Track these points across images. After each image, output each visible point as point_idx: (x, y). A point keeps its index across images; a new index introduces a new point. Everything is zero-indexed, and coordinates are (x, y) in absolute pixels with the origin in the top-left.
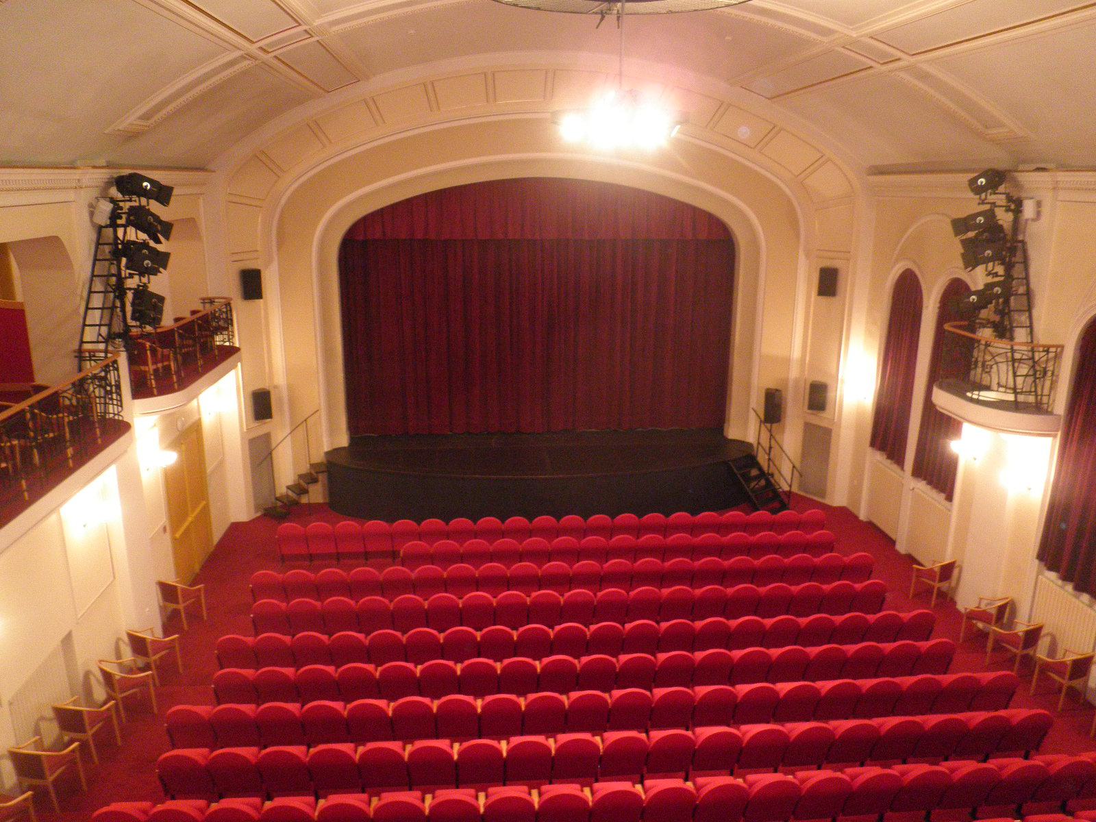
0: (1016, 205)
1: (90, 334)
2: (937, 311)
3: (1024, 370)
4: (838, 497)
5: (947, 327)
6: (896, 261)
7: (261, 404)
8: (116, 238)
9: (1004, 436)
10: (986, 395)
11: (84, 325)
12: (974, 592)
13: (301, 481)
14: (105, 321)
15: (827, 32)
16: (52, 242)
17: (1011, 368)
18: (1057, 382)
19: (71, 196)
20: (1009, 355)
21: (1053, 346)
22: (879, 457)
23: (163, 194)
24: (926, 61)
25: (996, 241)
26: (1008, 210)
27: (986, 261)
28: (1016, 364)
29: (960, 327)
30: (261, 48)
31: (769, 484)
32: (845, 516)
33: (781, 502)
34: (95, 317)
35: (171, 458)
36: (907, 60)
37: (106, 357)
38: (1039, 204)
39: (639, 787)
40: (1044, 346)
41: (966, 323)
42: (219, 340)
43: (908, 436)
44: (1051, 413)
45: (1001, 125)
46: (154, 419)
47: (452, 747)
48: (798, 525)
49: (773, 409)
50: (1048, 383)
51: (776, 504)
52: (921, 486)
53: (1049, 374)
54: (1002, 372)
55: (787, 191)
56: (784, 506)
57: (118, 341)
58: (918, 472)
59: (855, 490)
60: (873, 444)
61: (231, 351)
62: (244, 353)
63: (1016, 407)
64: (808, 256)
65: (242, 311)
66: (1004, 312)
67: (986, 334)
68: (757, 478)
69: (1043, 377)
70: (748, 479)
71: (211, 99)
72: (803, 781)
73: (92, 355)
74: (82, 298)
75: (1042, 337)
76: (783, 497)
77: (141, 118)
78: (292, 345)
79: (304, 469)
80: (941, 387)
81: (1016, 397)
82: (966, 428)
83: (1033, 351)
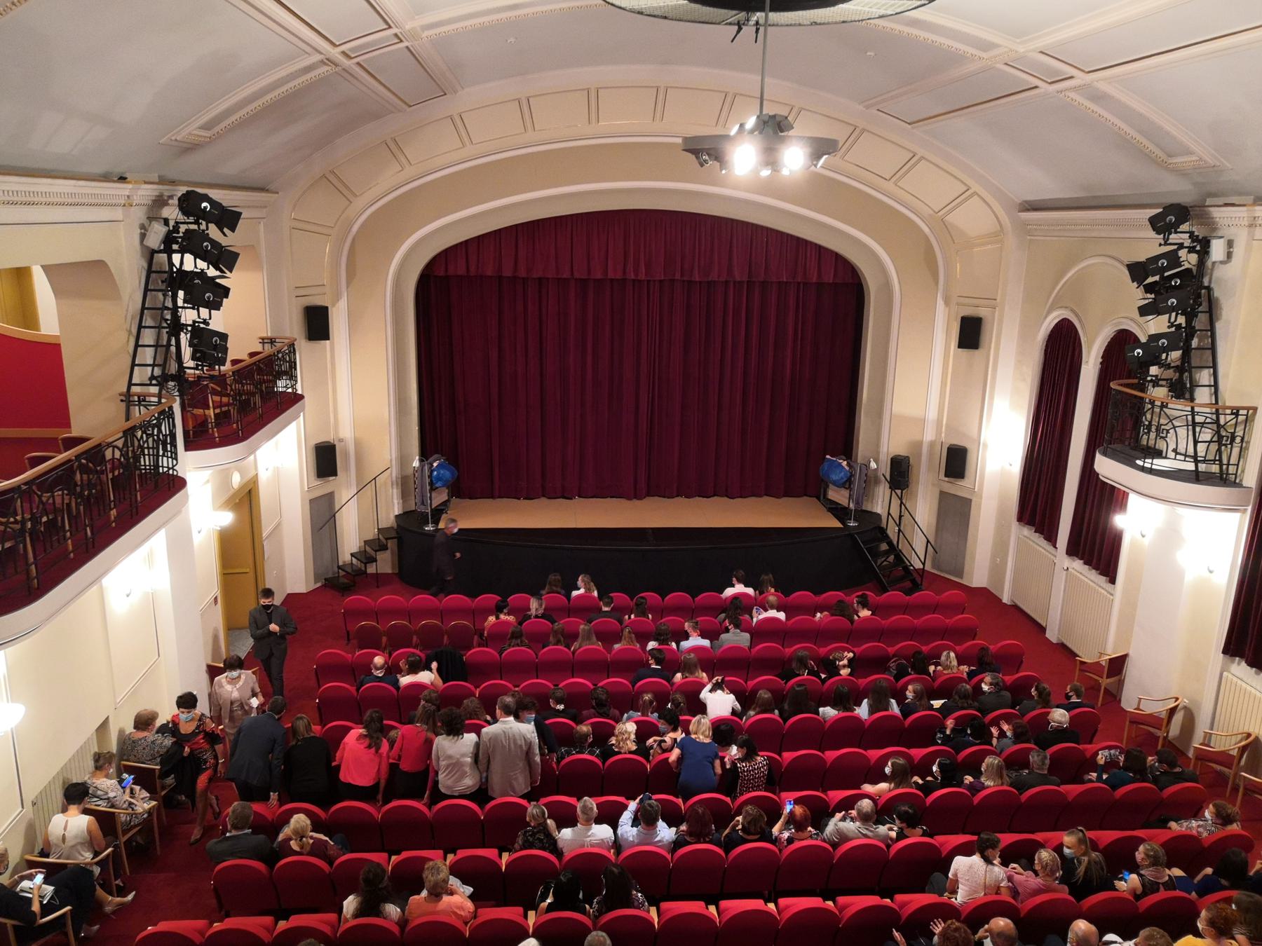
0: (1202, 246)
1: (140, 375)
2: (1099, 366)
3: (1206, 435)
4: (977, 577)
5: (1113, 385)
6: (1049, 313)
7: (326, 460)
8: (171, 264)
9: (1181, 511)
10: (1159, 464)
11: (133, 365)
12: (1145, 691)
13: (368, 549)
14: (160, 361)
15: (987, 46)
16: (98, 267)
17: (1191, 433)
18: (1247, 448)
19: (118, 214)
20: (1190, 418)
21: (1243, 408)
22: (1027, 532)
23: (228, 219)
24: (1104, 79)
25: (1182, 290)
26: (1191, 250)
27: (1172, 309)
28: (1198, 429)
29: (1127, 386)
30: (343, 53)
31: (899, 558)
32: (986, 597)
33: (913, 581)
34: (147, 355)
35: (227, 518)
36: (1081, 79)
37: (160, 402)
38: (1230, 244)
39: (712, 909)
40: (1232, 408)
41: (1136, 381)
42: (281, 385)
43: (1068, 509)
44: (1240, 485)
45: (1189, 152)
46: (207, 473)
47: (500, 857)
48: (935, 608)
49: (900, 473)
50: (1236, 451)
51: (908, 584)
52: (1077, 565)
53: (1238, 440)
54: (1181, 438)
55: (926, 230)
56: (915, 587)
57: (171, 384)
58: (1074, 550)
59: (997, 570)
60: (1020, 519)
61: (297, 398)
62: (307, 400)
63: (1196, 477)
64: (947, 302)
65: (306, 354)
66: (1185, 367)
67: (1160, 393)
68: (887, 553)
69: (1231, 444)
70: (876, 554)
71: (282, 108)
72: (902, 905)
73: (142, 400)
74: (130, 332)
75: (1230, 398)
76: (915, 575)
77: (201, 128)
78: (361, 390)
79: (371, 534)
80: (1105, 454)
81: (1197, 467)
82: (1133, 500)
83: (1217, 413)
